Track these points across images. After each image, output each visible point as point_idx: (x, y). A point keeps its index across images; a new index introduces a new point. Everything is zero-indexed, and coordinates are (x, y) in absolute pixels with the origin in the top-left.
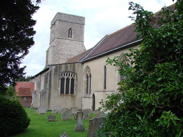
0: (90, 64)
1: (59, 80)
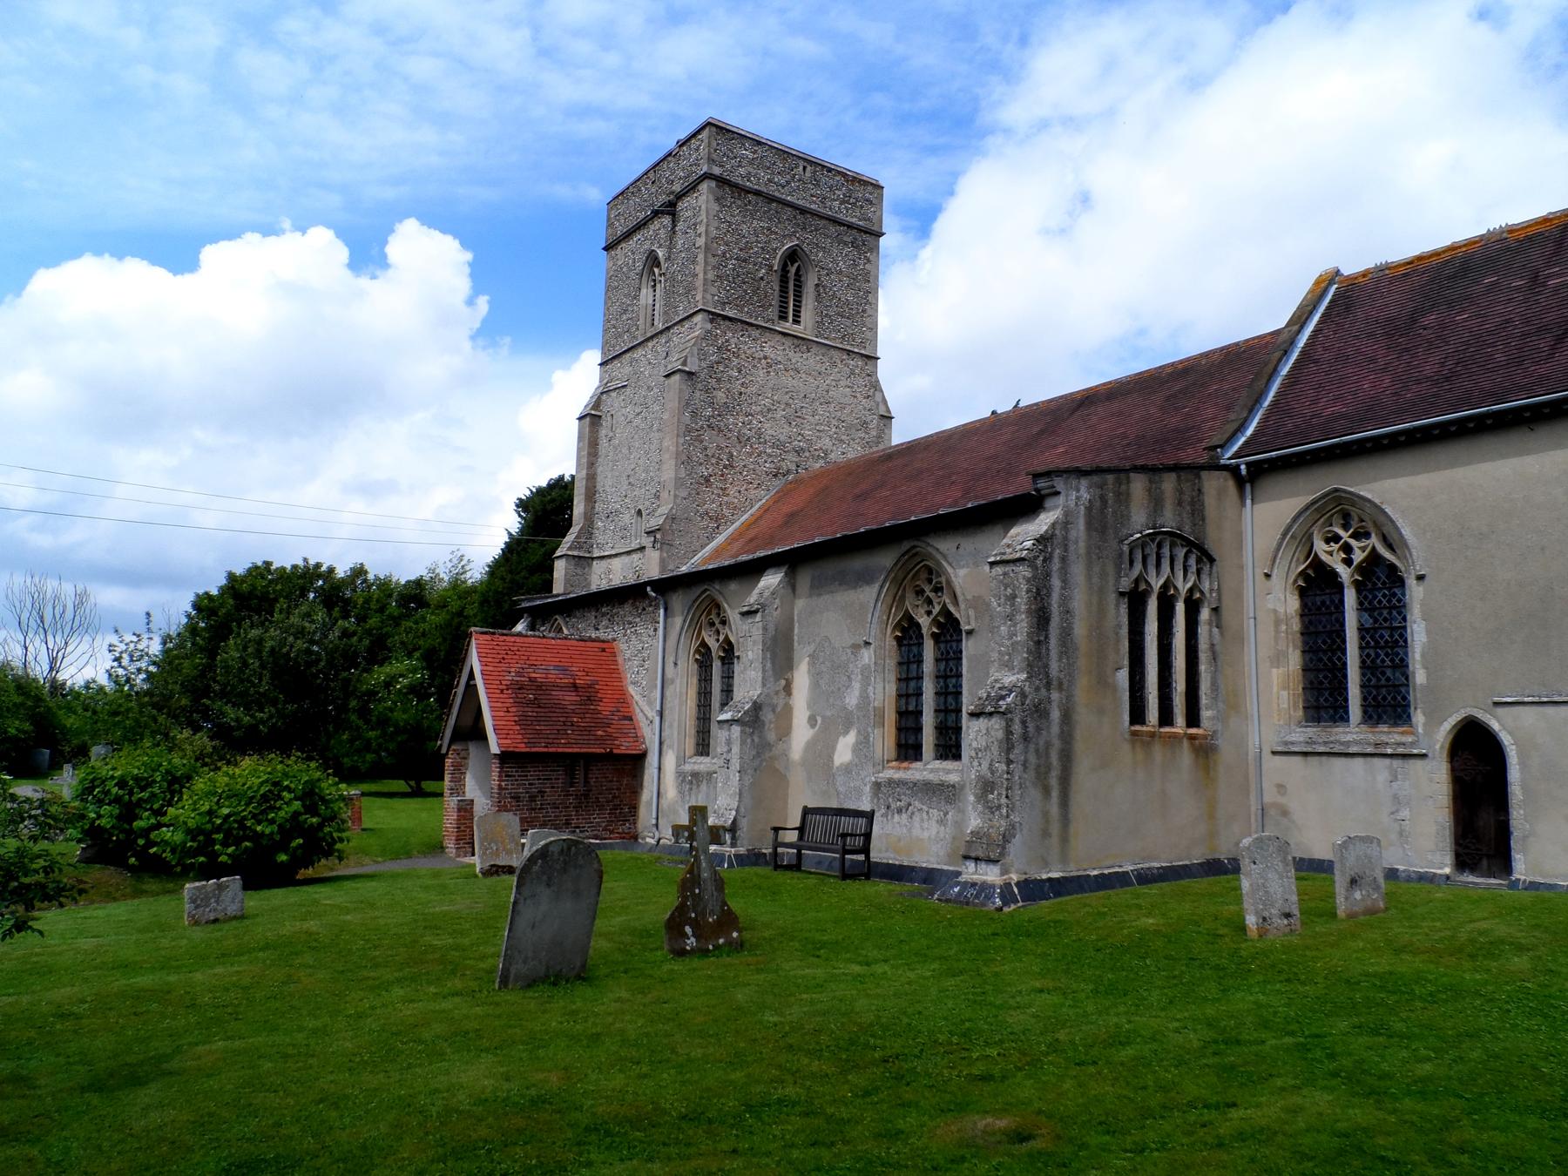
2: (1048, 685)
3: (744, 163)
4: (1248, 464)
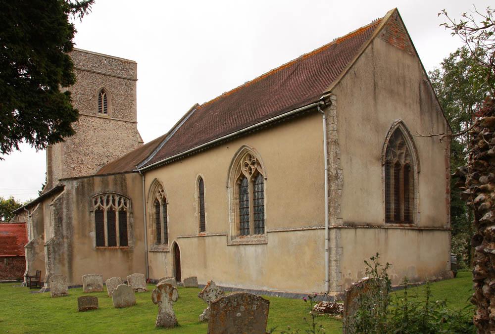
0: (164, 176)
1: (90, 215)
2: (63, 237)
3: (82, 61)
4: (141, 171)
